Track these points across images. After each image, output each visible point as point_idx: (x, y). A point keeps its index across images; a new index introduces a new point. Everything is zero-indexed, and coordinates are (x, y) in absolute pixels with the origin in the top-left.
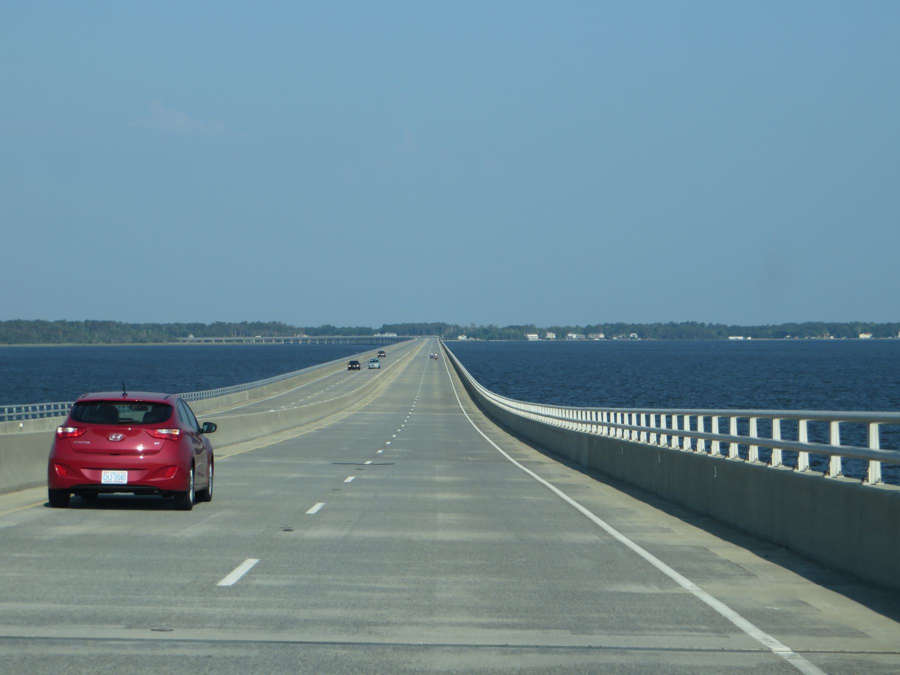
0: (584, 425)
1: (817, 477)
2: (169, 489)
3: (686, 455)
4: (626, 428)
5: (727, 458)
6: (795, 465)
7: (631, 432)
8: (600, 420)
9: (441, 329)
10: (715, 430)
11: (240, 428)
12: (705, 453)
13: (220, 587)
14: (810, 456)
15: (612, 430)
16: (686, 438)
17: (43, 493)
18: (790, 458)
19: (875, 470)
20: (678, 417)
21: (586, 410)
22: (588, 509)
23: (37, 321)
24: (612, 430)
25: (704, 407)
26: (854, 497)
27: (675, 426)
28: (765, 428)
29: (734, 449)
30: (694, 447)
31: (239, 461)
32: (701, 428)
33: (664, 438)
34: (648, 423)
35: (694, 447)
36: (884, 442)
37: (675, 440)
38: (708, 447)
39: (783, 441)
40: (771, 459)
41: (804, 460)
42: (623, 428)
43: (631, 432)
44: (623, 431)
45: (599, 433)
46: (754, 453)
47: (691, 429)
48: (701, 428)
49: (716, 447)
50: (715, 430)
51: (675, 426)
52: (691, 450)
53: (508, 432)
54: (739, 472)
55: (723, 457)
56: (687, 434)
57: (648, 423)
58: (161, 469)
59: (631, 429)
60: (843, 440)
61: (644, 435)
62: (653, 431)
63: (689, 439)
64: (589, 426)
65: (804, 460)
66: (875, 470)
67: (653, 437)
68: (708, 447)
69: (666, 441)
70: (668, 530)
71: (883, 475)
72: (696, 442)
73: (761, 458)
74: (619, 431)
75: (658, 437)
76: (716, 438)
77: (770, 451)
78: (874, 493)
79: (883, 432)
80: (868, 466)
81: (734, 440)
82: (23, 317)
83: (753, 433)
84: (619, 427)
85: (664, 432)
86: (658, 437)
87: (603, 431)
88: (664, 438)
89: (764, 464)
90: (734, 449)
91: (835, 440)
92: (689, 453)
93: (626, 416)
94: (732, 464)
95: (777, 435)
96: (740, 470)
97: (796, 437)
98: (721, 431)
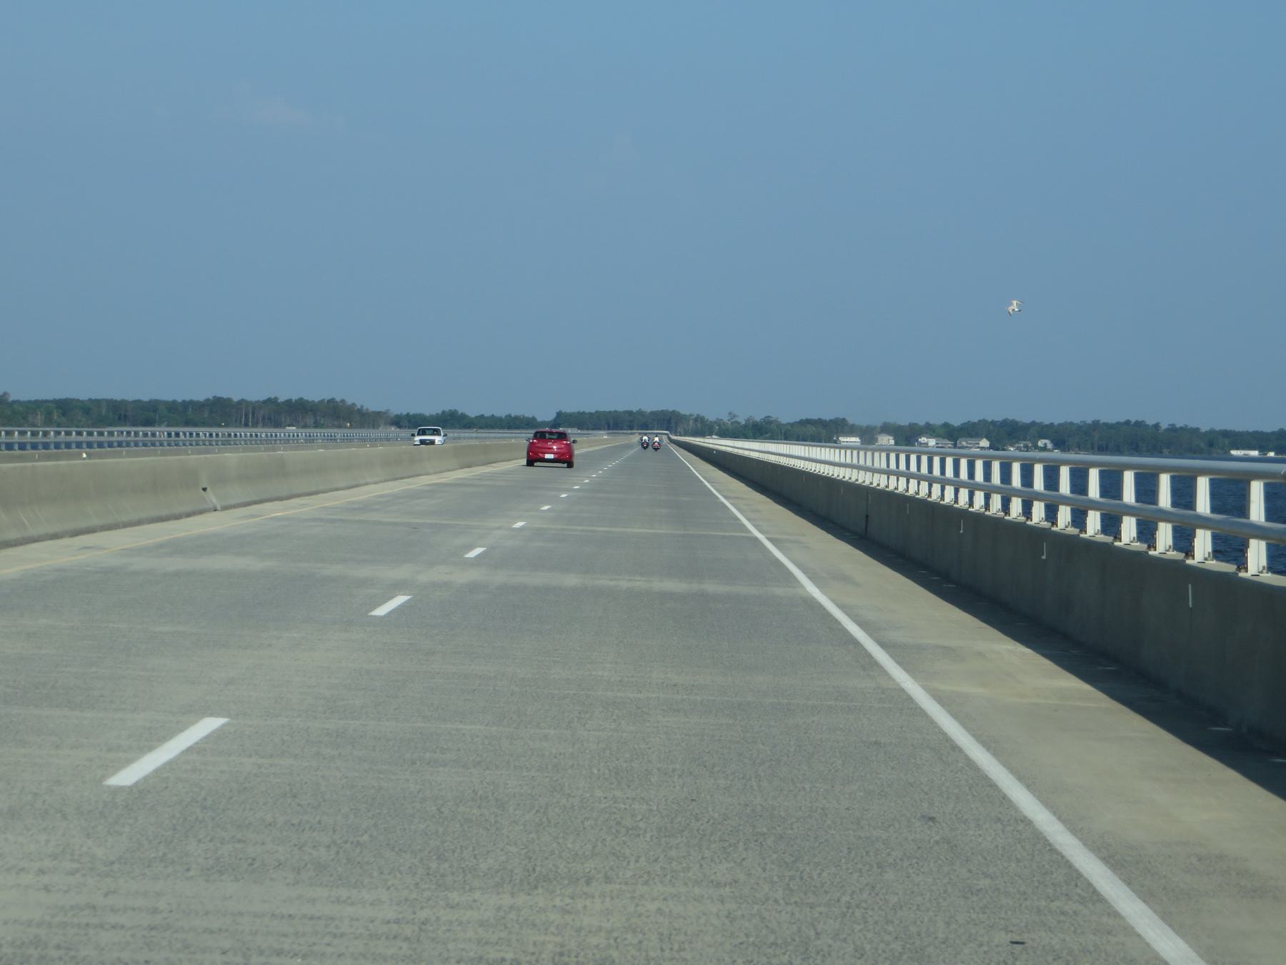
0: (862, 472)
1: (1226, 574)
2: (566, 460)
3: (1015, 526)
6: (1117, 536)
7: (930, 486)
9: (669, 421)
10: (1065, 487)
11: (585, 444)
12: (1022, 519)
13: (109, 787)
14: (1215, 538)
15: (913, 483)
16: (977, 493)
17: (524, 462)
18: (1111, 524)
19: (1257, 554)
20: (1002, 465)
22: (955, 715)
24: (893, 478)
25: (1102, 449)
26: (1227, 591)
27: (979, 477)
28: (1111, 486)
29: (1064, 515)
31: (581, 455)
32: (1016, 481)
34: (987, 476)
35: (987, 506)
36: (1272, 512)
39: (1173, 510)
41: (1203, 543)
42: (920, 478)
43: (930, 486)
44: (908, 482)
45: (891, 488)
46: (1094, 522)
47: (1046, 487)
48: (1016, 481)
49: (1038, 510)
50: (1065, 487)
52: (1022, 519)
53: (828, 530)
54: (1072, 549)
55: (1180, 556)
57: (987, 476)
58: (563, 454)
59: (944, 483)
60: (1271, 514)
61: (949, 491)
63: (982, 494)
65: (1203, 543)
66: (1257, 554)
69: (983, 503)
71: (1073, 521)
76: (1039, 497)
77: (1085, 514)
78: (1255, 588)
79: (1270, 496)
80: (1156, 529)
81: (1165, 516)
83: (1094, 491)
85: (997, 490)
86: (987, 498)
87: (880, 481)
90: (1064, 515)
91: (1257, 511)
92: (1019, 524)
93: (903, 457)
94: (1161, 563)
95: (1129, 495)
96: (1072, 547)
98: (1104, 493)
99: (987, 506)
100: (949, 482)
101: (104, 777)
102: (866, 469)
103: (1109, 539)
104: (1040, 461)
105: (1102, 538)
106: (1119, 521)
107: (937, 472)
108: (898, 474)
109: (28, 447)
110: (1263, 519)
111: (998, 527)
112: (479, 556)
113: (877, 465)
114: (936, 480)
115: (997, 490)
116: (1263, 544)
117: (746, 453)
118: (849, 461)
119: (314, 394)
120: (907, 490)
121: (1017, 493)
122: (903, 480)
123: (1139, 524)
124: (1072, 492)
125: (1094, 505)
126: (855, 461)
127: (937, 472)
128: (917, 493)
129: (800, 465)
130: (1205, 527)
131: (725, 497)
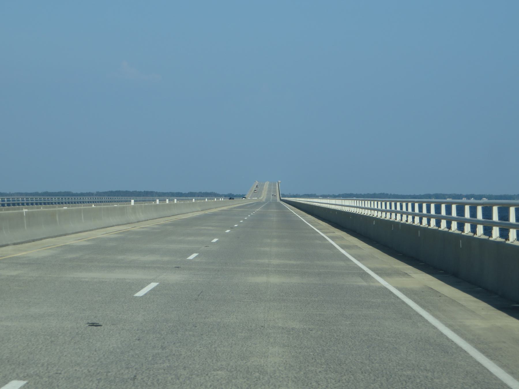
0: (366, 210)
4: (399, 212)
5: (440, 229)
6: (507, 238)
7: (402, 216)
8: (372, 207)
10: (454, 213)
12: (447, 230)
15: (393, 215)
16: (416, 217)
19: (513, 234)
20: (412, 204)
21: (374, 201)
23: (126, 191)
24: (380, 213)
27: (425, 211)
29: (480, 229)
30: (421, 222)
33: (425, 220)
34: (413, 209)
35: (421, 222)
37: (425, 220)
38: (449, 226)
39: (499, 221)
40: (464, 229)
42: (382, 211)
45: (379, 216)
47: (436, 213)
49: (454, 225)
50: (454, 213)
51: (425, 211)
52: (447, 230)
56: (433, 217)
57: (413, 209)
59: (396, 213)
62: (417, 215)
63: (418, 217)
64: (376, 212)
67: (417, 219)
68: (449, 226)
70: (406, 275)
71: (458, 227)
72: (451, 223)
73: (501, 236)
74: (384, 214)
75: (413, 218)
77: (508, 231)
78: (512, 247)
82: (121, 190)
84: (388, 211)
86: (413, 218)
88: (425, 220)
89: (503, 240)
92: (445, 232)
94: (480, 240)
97: (463, 215)
99: (413, 221)
100: (399, 212)
101: (27, 383)
102: (362, 208)
103: (486, 237)
104: (417, 202)
105: (500, 240)
106: (464, 225)
107: (393, 208)
108: (386, 211)
109: (11, 205)
110: (469, 217)
111: (426, 231)
112: (191, 255)
113: (366, 206)
114: (393, 212)
115: (417, 215)
116: (434, 219)
117: (314, 204)
118: (355, 205)
119: (209, 191)
120: (386, 217)
121: (444, 218)
122: (384, 214)
123: (458, 224)
124: (483, 218)
125: (496, 224)
126: (358, 205)
127: (393, 208)
128: (381, 217)
129: (333, 207)
130: (496, 226)
131: (343, 247)
